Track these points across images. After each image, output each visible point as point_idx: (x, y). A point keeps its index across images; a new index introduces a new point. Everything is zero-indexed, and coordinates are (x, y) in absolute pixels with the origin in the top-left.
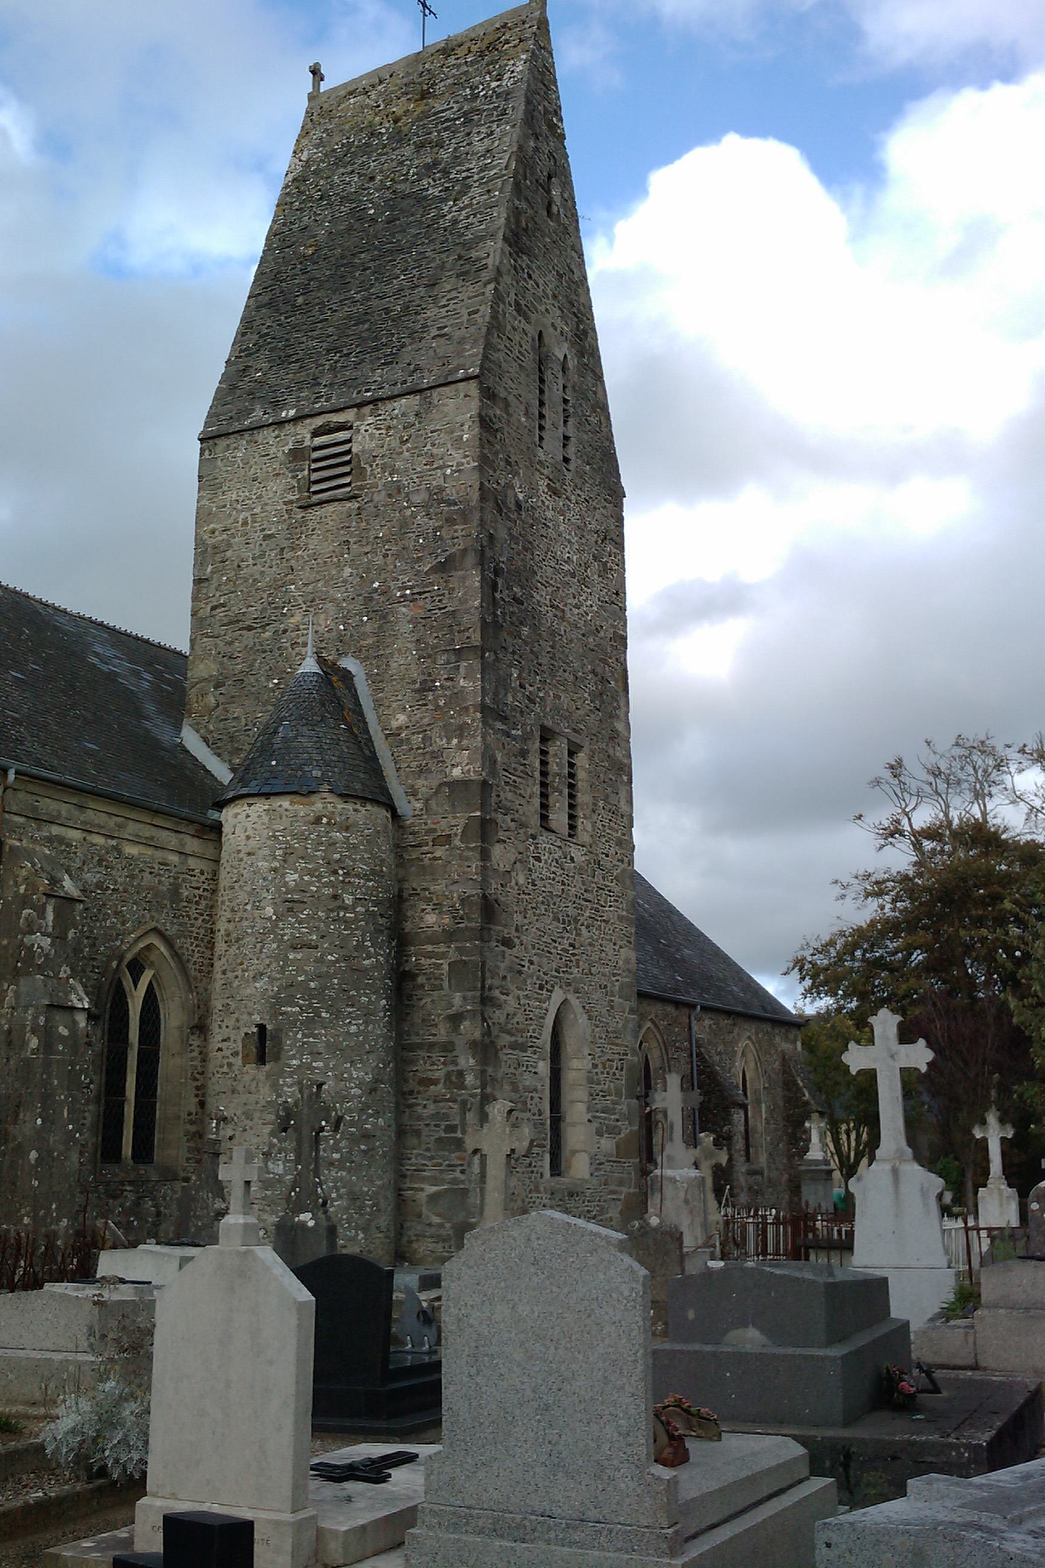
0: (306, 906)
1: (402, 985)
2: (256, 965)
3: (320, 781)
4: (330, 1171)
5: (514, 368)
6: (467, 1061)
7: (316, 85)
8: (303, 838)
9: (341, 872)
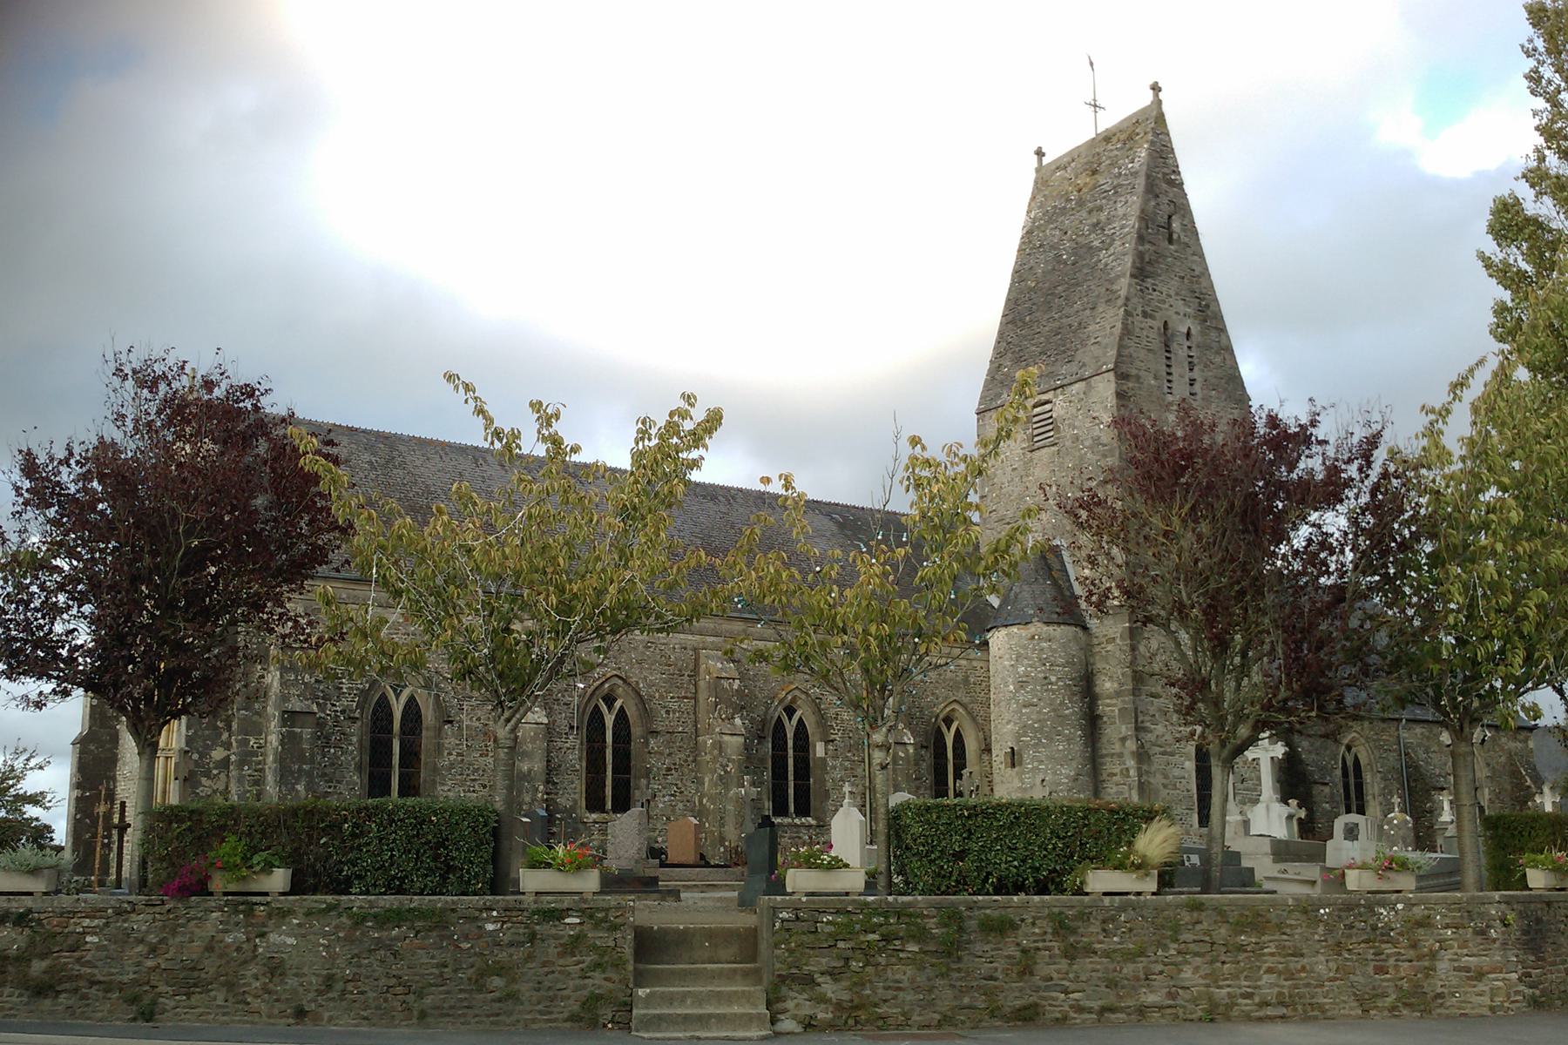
2: (1007, 716)
3: (1033, 616)
5: (1142, 354)
6: (1131, 763)
7: (1040, 161)
8: (1025, 647)
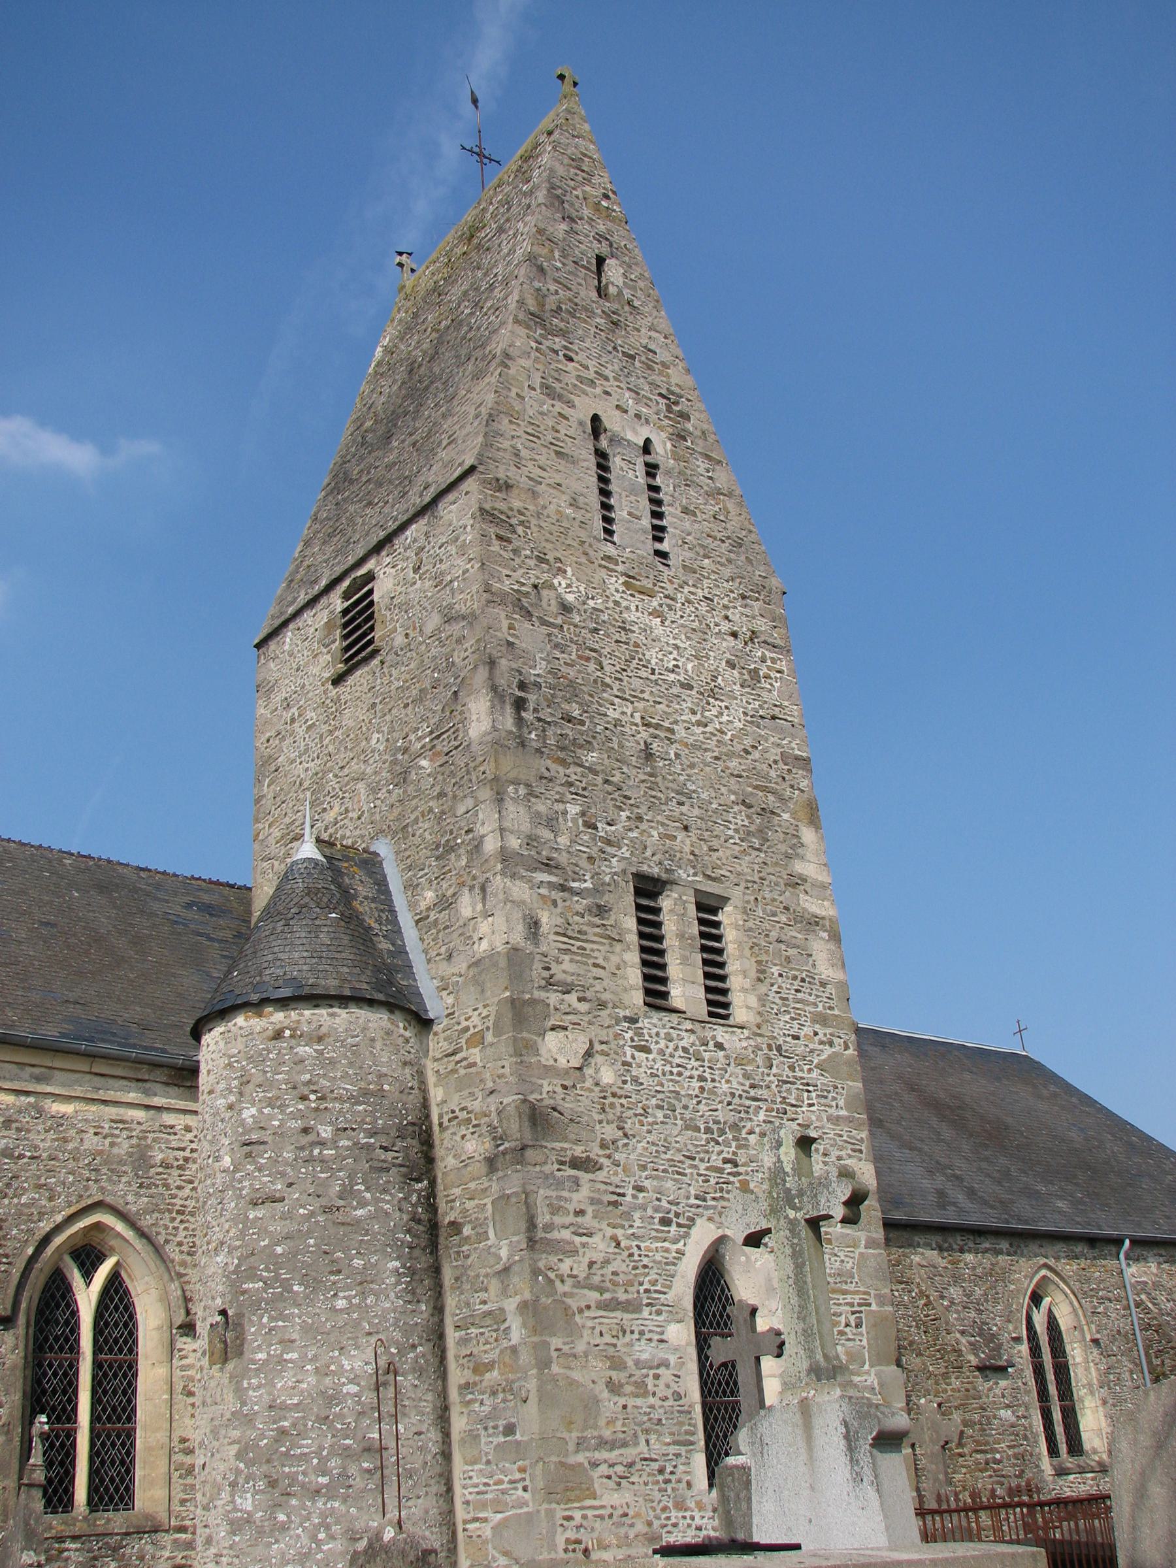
0: (267, 1147)
1: (430, 1234)
4: (314, 1502)
8: (258, 1059)
9: (313, 1097)
